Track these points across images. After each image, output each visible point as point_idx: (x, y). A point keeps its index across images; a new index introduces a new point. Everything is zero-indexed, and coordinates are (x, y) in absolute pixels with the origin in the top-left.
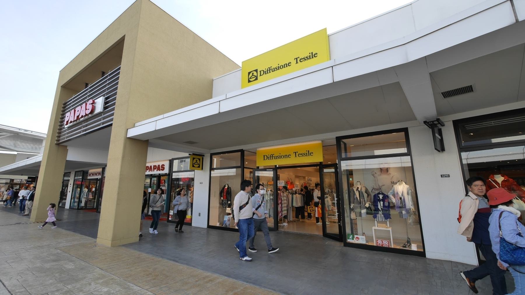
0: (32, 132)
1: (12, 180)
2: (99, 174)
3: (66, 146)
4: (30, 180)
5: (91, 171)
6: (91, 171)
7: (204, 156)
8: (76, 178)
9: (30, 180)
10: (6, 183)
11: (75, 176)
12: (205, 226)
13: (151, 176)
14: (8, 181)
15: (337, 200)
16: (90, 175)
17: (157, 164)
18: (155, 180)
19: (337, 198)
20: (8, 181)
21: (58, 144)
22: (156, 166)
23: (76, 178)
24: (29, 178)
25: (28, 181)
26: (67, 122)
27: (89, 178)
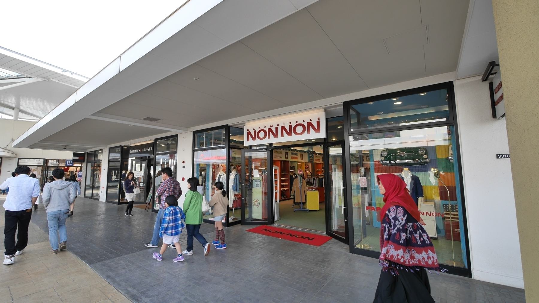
1: (46, 161)
4: (77, 158)
5: (251, 126)
6: (251, 126)
9: (77, 158)
14: (41, 163)
24: (75, 155)
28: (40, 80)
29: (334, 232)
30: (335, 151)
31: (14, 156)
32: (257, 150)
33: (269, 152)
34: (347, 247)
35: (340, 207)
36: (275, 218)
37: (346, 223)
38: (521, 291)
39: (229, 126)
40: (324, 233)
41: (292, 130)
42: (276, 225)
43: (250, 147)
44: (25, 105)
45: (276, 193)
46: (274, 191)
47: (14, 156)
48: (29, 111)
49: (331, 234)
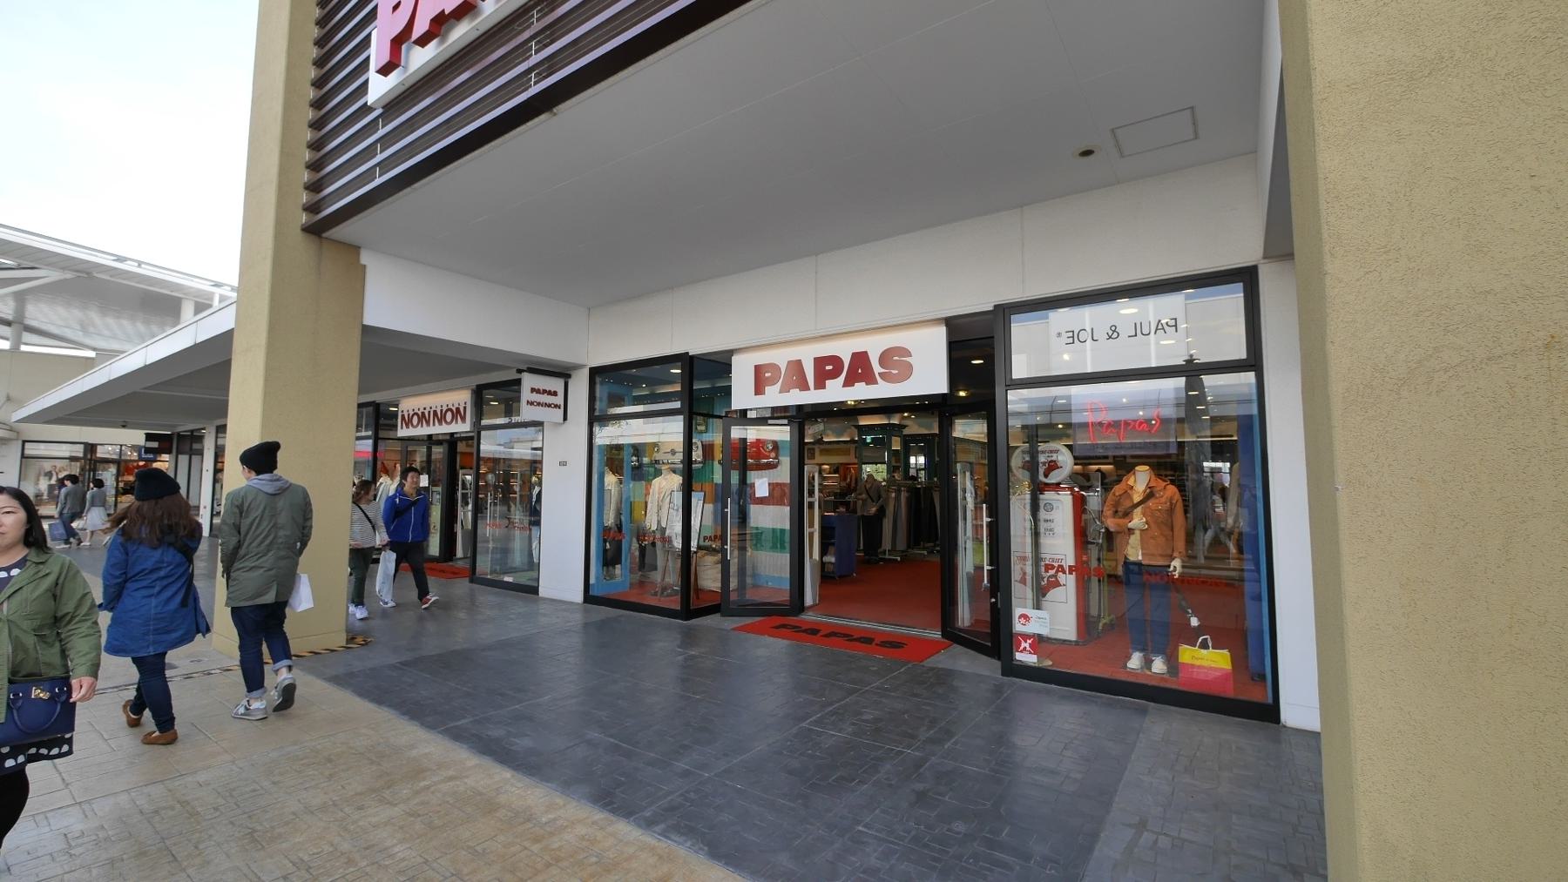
0: (140, 264)
1: (91, 448)
2: (458, 414)
3: (354, 249)
4: (155, 445)
5: (409, 405)
6: (409, 405)
7: (569, 376)
8: (607, 435)
9: (155, 445)
10: (73, 459)
11: (596, 418)
12: (578, 597)
13: (430, 440)
14: (79, 451)
15: (989, 524)
16: (408, 423)
17: (844, 350)
18: (438, 452)
19: (989, 516)
20: (79, 451)
21: (316, 230)
22: (836, 361)
23: (607, 435)
24: (149, 437)
25: (148, 450)
26: (398, 42)
27: (403, 432)
28: (69, 275)
29: (960, 630)
30: (969, 429)
31: (13, 435)
32: (761, 421)
33: (796, 426)
34: (997, 664)
35: (979, 568)
36: (809, 600)
37: (993, 606)
38: (1316, 735)
39: (692, 357)
40: (936, 635)
41: (441, 418)
42: (809, 617)
43: (744, 412)
44: (37, 314)
45: (811, 535)
46: (807, 531)
47: (13, 435)
48: (44, 327)
49: (953, 635)
